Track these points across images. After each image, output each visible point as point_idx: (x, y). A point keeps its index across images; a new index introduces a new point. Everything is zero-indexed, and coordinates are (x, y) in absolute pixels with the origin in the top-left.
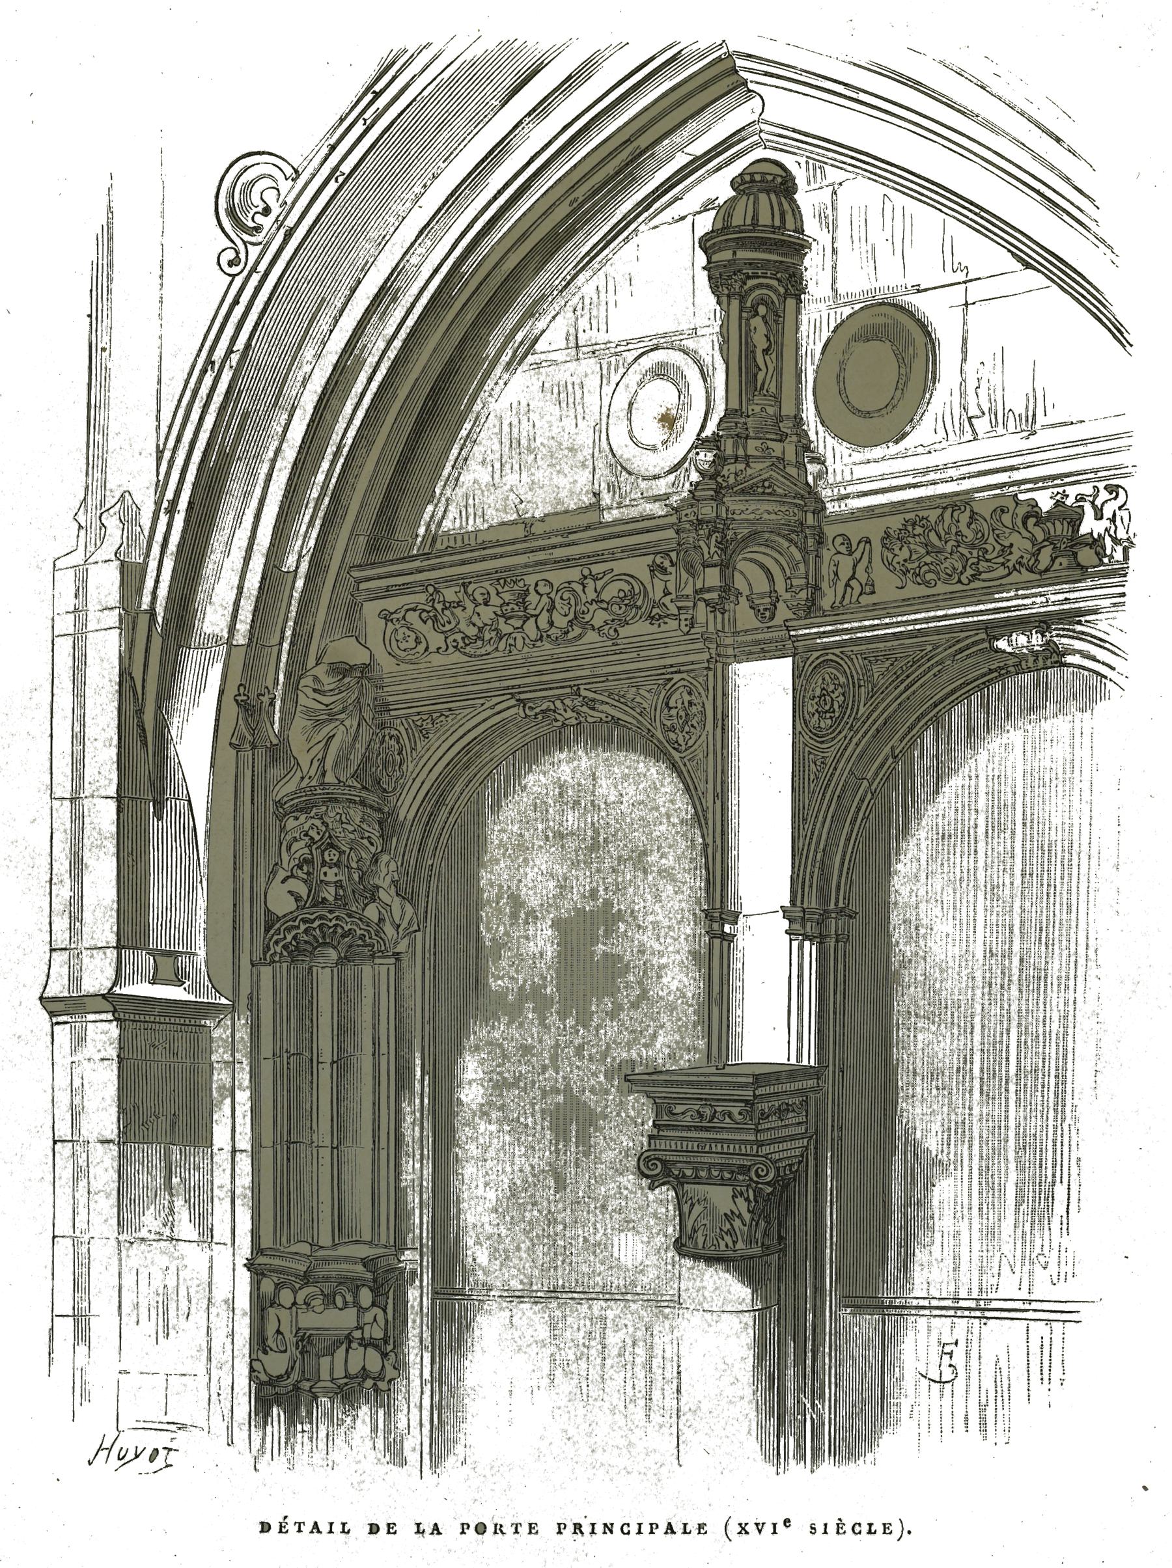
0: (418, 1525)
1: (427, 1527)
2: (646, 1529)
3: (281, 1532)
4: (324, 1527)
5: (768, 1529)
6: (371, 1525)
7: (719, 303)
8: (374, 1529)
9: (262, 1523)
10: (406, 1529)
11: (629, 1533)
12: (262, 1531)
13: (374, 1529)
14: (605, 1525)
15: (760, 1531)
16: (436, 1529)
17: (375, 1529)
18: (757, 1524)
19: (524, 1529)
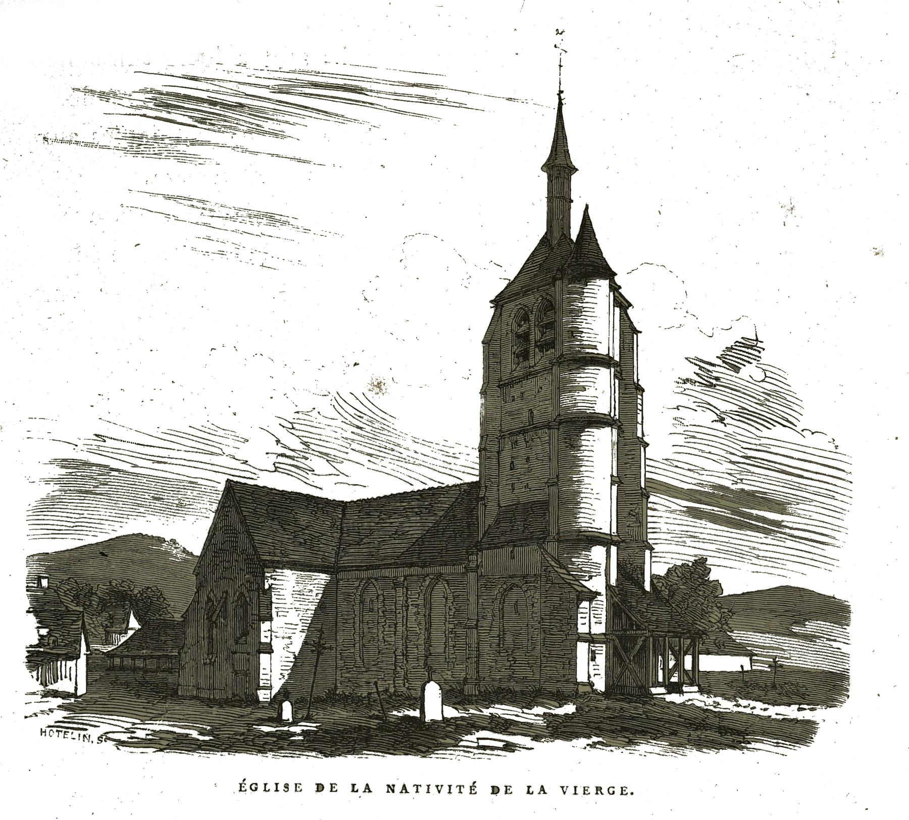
0: (353, 785)
1: (536, 789)
2: (281, 787)
3: (622, 794)
4: (433, 789)
5: (422, 790)
6: (318, 785)
7: (448, 486)
8: (320, 788)
9: (493, 787)
10: (519, 790)
11: (614, 793)
12: (318, 791)
13: (320, 788)
14: (388, 786)
15: (439, 792)
16: (368, 789)
17: (320, 787)
18: (437, 786)
19: (398, 788)
